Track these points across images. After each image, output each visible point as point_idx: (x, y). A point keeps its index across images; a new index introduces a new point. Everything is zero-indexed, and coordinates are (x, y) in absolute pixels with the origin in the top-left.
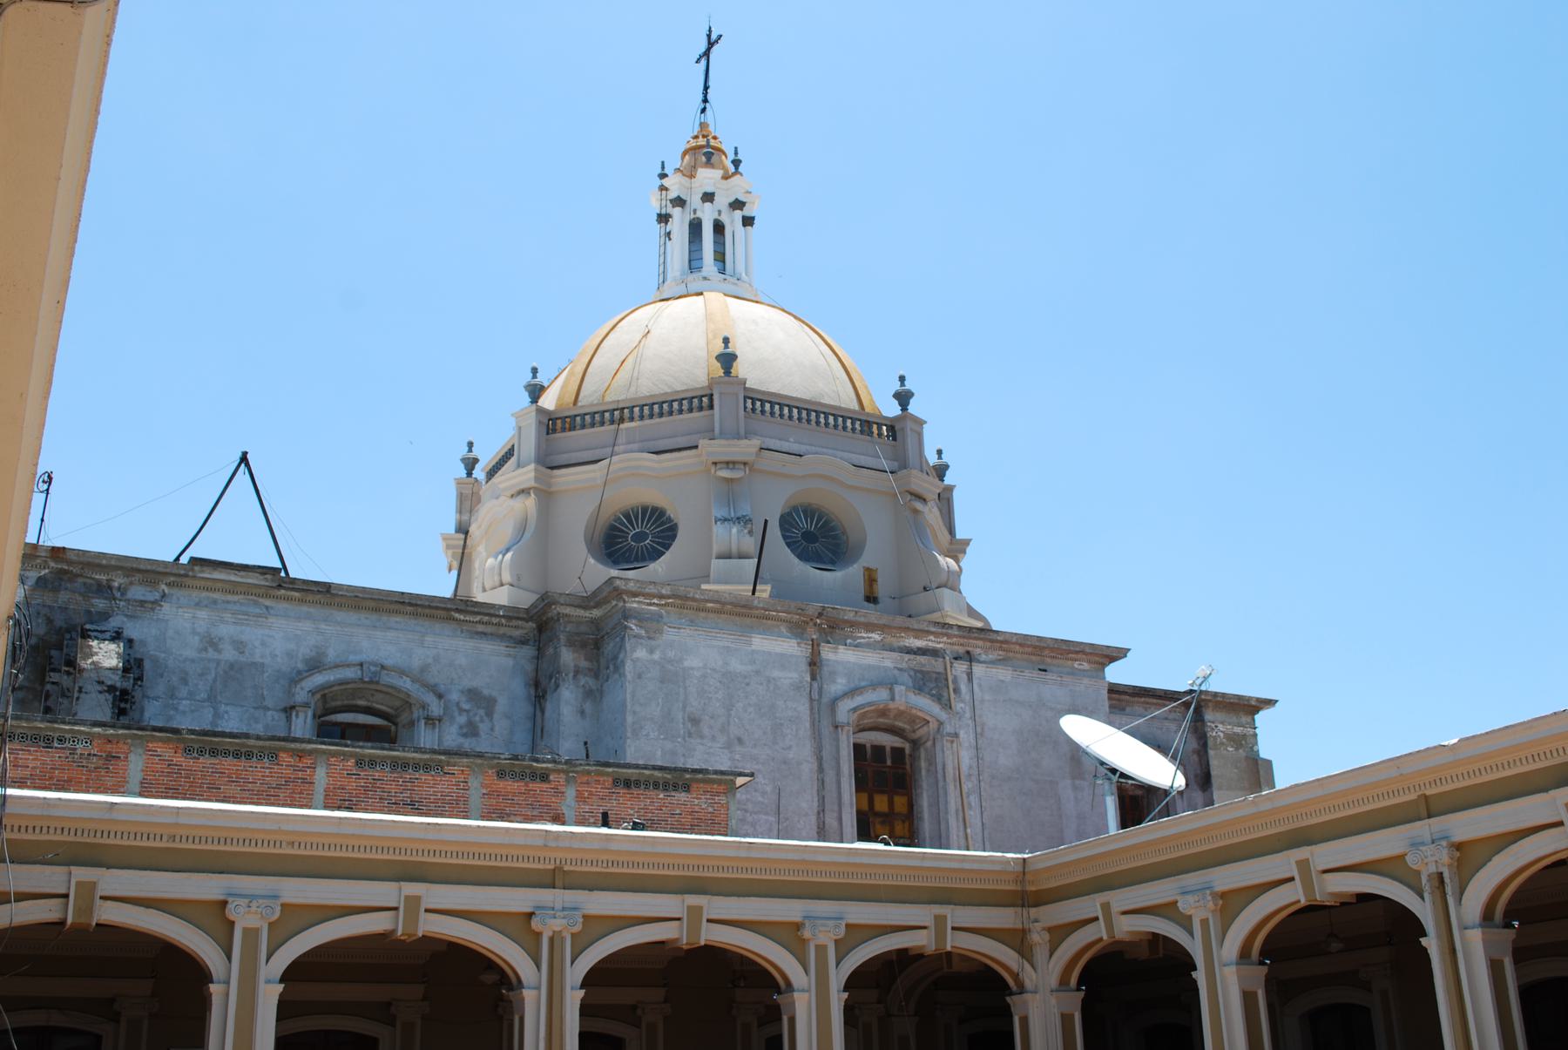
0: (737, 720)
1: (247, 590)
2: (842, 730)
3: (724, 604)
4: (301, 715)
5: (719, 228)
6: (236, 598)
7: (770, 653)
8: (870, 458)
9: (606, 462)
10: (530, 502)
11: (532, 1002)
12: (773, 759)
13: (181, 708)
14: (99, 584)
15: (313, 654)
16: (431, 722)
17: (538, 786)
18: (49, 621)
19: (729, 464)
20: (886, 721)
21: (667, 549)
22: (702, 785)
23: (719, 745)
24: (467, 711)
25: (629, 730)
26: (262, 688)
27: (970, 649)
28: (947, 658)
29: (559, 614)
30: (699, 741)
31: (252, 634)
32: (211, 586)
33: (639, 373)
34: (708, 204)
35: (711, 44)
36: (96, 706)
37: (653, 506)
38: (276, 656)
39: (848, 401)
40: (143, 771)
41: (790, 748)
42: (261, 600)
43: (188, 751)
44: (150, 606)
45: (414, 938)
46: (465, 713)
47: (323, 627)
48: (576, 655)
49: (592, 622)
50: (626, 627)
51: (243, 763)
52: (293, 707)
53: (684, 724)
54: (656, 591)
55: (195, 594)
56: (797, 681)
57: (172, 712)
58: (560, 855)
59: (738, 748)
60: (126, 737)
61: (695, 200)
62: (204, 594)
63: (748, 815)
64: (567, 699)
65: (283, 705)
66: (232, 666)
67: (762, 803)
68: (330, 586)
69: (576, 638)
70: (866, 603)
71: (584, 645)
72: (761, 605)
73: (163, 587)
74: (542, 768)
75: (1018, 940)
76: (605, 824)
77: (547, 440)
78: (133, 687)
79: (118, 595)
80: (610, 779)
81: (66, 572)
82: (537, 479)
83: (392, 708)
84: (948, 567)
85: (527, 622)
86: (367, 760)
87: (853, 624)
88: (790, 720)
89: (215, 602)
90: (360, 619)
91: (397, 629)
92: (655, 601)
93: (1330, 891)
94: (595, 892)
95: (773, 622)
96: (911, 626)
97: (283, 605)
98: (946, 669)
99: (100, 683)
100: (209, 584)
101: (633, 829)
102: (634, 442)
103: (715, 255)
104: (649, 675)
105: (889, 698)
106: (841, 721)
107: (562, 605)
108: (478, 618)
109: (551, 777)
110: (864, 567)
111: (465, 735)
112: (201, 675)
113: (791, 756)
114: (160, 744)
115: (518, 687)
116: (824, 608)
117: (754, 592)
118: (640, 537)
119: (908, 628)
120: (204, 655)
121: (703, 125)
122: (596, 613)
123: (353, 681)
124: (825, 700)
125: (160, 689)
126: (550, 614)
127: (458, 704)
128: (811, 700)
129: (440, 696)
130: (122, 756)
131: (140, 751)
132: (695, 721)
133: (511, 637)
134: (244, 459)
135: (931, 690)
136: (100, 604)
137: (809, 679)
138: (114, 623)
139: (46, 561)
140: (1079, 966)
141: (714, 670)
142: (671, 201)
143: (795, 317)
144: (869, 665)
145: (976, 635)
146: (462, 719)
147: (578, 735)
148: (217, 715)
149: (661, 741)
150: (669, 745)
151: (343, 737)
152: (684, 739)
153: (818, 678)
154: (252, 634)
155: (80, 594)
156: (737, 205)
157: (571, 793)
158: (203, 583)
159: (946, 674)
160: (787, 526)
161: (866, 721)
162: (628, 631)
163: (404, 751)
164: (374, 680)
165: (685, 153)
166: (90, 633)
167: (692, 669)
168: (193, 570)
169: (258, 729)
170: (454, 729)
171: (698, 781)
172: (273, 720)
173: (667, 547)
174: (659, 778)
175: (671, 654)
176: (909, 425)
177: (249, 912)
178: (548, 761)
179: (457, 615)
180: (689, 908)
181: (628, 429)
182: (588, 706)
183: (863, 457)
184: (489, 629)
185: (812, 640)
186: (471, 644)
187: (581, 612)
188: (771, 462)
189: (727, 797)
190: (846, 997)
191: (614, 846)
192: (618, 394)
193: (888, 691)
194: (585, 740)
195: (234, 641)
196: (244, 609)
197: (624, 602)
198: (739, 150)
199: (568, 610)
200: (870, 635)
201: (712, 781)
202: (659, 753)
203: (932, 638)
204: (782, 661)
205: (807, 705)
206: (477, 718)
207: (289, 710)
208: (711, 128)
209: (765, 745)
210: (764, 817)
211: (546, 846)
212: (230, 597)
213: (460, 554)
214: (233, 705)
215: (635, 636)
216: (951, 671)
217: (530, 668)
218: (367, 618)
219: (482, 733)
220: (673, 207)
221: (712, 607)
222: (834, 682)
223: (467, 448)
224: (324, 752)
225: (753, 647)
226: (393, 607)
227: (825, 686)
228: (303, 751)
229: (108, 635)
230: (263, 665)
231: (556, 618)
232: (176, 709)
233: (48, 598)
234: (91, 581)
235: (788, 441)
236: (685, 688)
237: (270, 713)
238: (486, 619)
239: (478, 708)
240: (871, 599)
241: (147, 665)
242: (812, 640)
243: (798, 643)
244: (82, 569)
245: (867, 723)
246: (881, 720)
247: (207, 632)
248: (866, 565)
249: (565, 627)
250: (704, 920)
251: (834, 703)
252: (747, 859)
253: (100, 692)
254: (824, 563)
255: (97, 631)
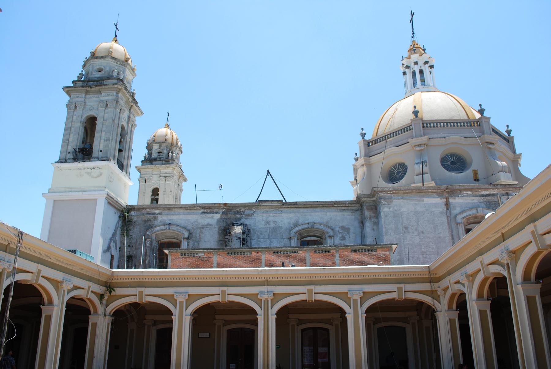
0: (421, 226)
1: (275, 207)
2: (459, 225)
3: (412, 190)
4: (293, 239)
5: (421, 72)
6: (273, 209)
7: (431, 203)
8: (471, 134)
9: (383, 152)
10: (365, 168)
11: (350, 318)
12: (435, 237)
13: (261, 241)
14: (238, 211)
15: (295, 222)
16: (330, 237)
17: (327, 254)
18: (226, 222)
19: (419, 145)
20: (478, 220)
21: (405, 175)
22: (380, 249)
23: (415, 235)
24: (342, 233)
25: (384, 233)
26: (282, 233)
27: (507, 192)
28: (498, 196)
29: (363, 201)
30: (408, 234)
31: (278, 219)
32: (265, 207)
33: (394, 122)
34: (416, 65)
35: (412, 15)
36: (236, 244)
37: (401, 163)
38: (285, 224)
39: (464, 117)
40: (217, 260)
41: (441, 233)
42: (280, 209)
43: (228, 254)
44: (251, 215)
45: (403, 299)
46: (341, 234)
47: (297, 214)
48: (370, 212)
49: (374, 202)
50: (380, 202)
51: (243, 256)
52: (291, 238)
53: (402, 229)
54: (388, 190)
55: (262, 210)
56: (442, 211)
57: (259, 243)
58: (266, 276)
59: (422, 235)
60: (213, 252)
61: (412, 65)
62: (264, 210)
63: (427, 256)
64: (368, 225)
65: (288, 237)
66: (273, 228)
67: (432, 251)
68: (297, 203)
69: (369, 207)
70: (474, 182)
71: (372, 209)
72: (425, 189)
73: (254, 209)
74: (328, 249)
75: (433, 294)
76: (283, 266)
77: (368, 149)
78: (247, 237)
79: (242, 213)
80: (350, 250)
81: (229, 209)
82: (365, 161)
83: (320, 234)
84: (502, 165)
85: (357, 204)
86: (276, 251)
87: (460, 190)
88: (440, 224)
89: (267, 211)
90: (307, 211)
91: (318, 212)
92: (389, 193)
93: (491, 272)
94: (277, 286)
95: (432, 193)
96: (481, 188)
97: (286, 210)
98: (498, 200)
99: (237, 237)
100: (265, 207)
101: (292, 267)
102: (392, 144)
103: (421, 80)
104: (389, 216)
105: (477, 212)
106: (458, 222)
107: (363, 198)
108: (342, 205)
109: (331, 251)
110: (472, 170)
111: (341, 240)
112: (266, 231)
113: (441, 235)
114: (221, 253)
115: (357, 224)
116: (447, 186)
117: (423, 185)
118: (398, 173)
119: (481, 188)
120: (266, 226)
121: (413, 41)
122: (374, 199)
123: (307, 228)
124: (452, 216)
125: (255, 237)
126: (361, 201)
127: (338, 231)
128: (447, 216)
129: (332, 230)
130: (212, 257)
131: (216, 255)
132: (406, 228)
133: (353, 209)
134: (268, 172)
135: (493, 207)
136: (238, 216)
137: (446, 210)
138: (242, 221)
139: (224, 207)
140: (92, 310)
141: (411, 211)
142: (405, 67)
143: (445, 93)
144: (468, 203)
145: (508, 187)
146: (340, 235)
147: (372, 236)
148: (271, 242)
149: (395, 236)
150: (398, 236)
151: (308, 245)
152: (403, 234)
153: (449, 209)
154: (278, 219)
155: (233, 214)
156: (426, 63)
157: (337, 255)
158: (263, 207)
159: (499, 202)
160: (444, 161)
161: (470, 221)
162: (381, 203)
163: (285, 248)
164: (312, 227)
165: (408, 52)
166: (234, 224)
167: (404, 212)
168: (260, 204)
169: (282, 245)
170: (338, 239)
171: (379, 248)
172: (286, 242)
173: (405, 174)
174: (366, 248)
175: (396, 208)
176: (483, 120)
177: (180, 297)
178: (329, 247)
179: (335, 205)
180: (308, 290)
181: (390, 141)
182: (375, 227)
183: (468, 134)
184: (346, 208)
185: (446, 197)
186: (341, 213)
187: (369, 199)
188: (433, 142)
189: (389, 252)
190: (365, 315)
191: (279, 273)
192: (387, 131)
193: (476, 210)
194: (375, 237)
195: (274, 221)
196: (275, 212)
197: (379, 194)
198: (424, 46)
199: (365, 199)
200: (467, 192)
201: (384, 248)
202: (395, 239)
203: (491, 190)
204: (436, 205)
205: (446, 218)
206: (345, 235)
207: (290, 238)
208: (416, 42)
209: (432, 233)
210: (434, 256)
211: (258, 274)
212: (271, 210)
213: (424, 182)
214: (275, 239)
215: (383, 204)
216: (500, 200)
217: (359, 218)
218: (309, 210)
219: (346, 239)
220: (406, 69)
221: (408, 192)
222: (455, 209)
223: (355, 155)
224: (264, 250)
225: (425, 202)
226: (316, 206)
227: (452, 211)
228: (258, 251)
229: (239, 224)
230: (282, 227)
231: (157, 214)
232: (260, 242)
233: (225, 217)
234: (236, 211)
235: (440, 134)
236: (402, 218)
237: (285, 240)
238: (344, 205)
239: (345, 231)
240: (476, 180)
241: (251, 230)
242: (446, 197)
243: (441, 199)
244: (233, 208)
245: (471, 221)
246: (476, 220)
247: (266, 220)
248: (474, 169)
249: (366, 204)
250: (226, 294)
251: (455, 217)
252: (291, 274)
253: (237, 239)
254: (459, 171)
255: (236, 223)
